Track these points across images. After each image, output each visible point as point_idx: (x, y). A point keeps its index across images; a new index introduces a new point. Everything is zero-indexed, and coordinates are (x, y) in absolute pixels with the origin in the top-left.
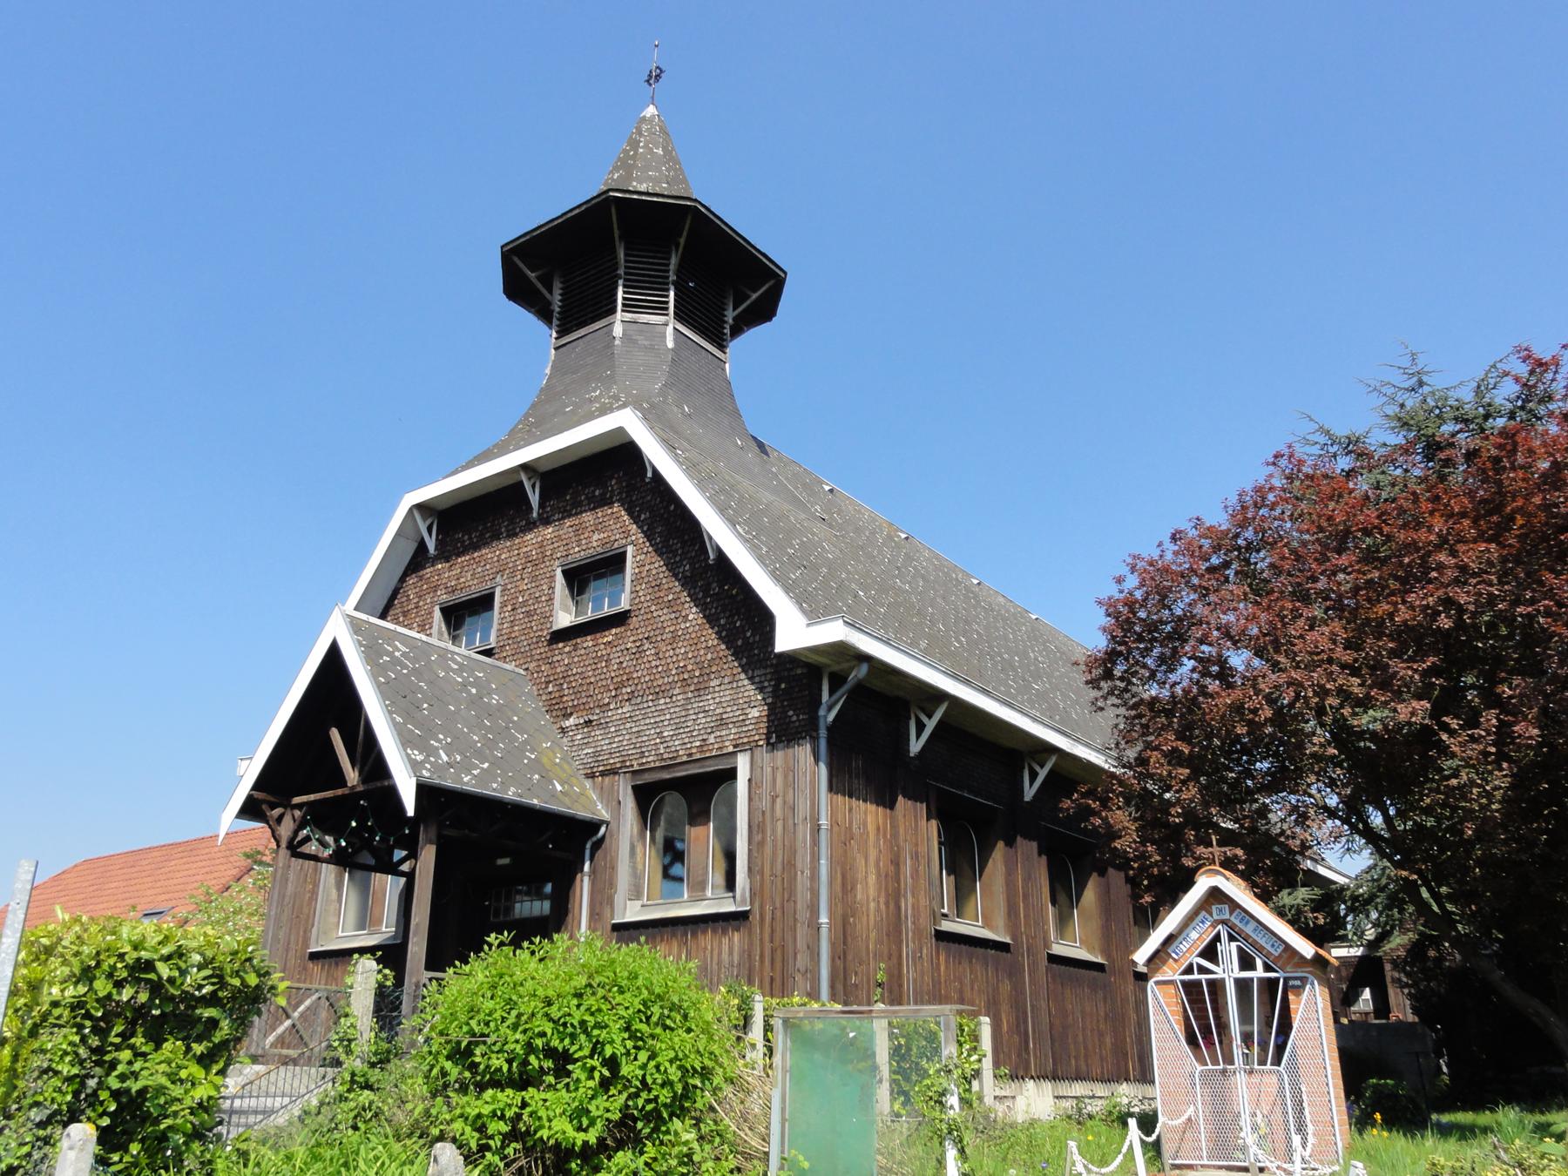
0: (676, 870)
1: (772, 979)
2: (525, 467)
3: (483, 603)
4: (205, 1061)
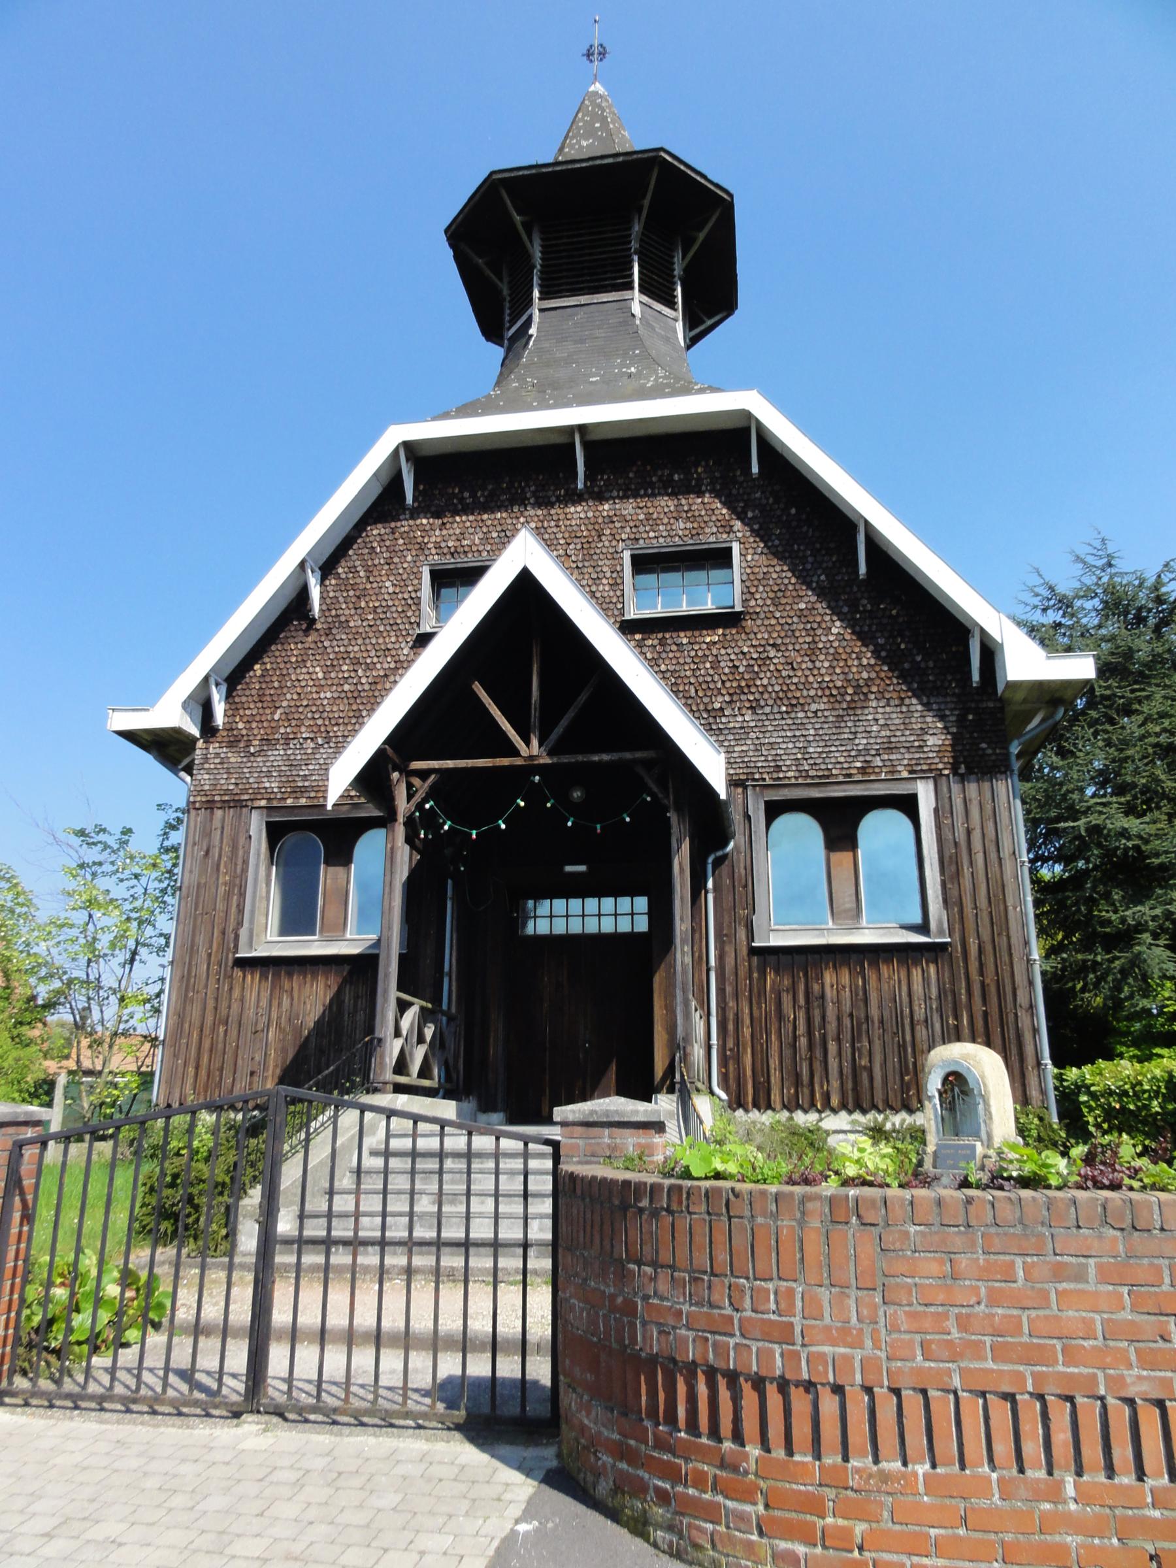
1: (986, 1014)
2: (582, 428)
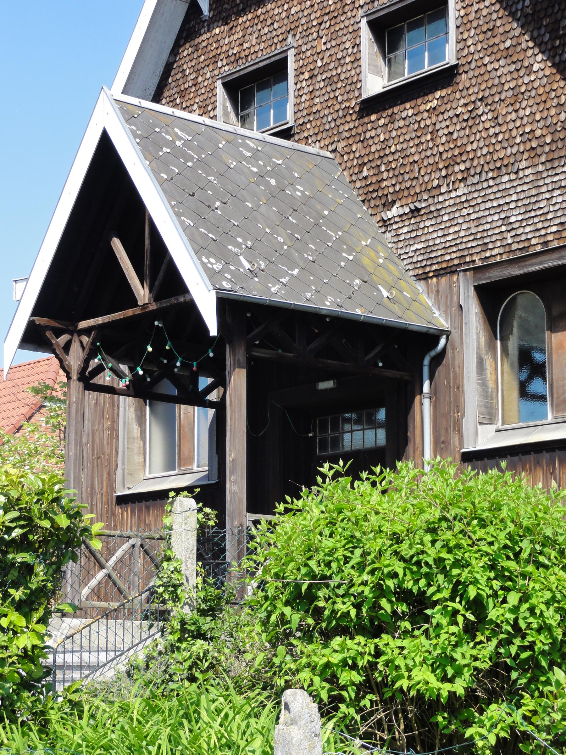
0: (536, 386)
3: (275, 71)
4: (24, 607)
